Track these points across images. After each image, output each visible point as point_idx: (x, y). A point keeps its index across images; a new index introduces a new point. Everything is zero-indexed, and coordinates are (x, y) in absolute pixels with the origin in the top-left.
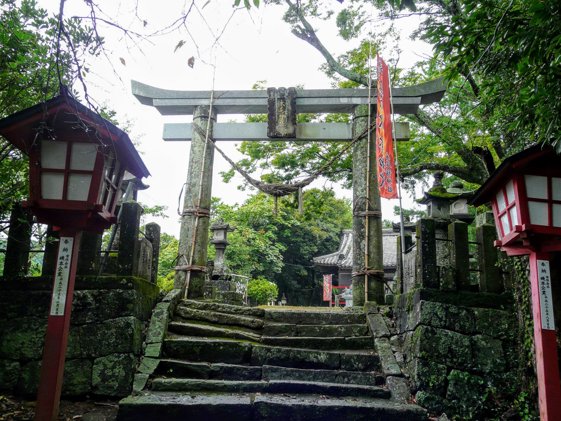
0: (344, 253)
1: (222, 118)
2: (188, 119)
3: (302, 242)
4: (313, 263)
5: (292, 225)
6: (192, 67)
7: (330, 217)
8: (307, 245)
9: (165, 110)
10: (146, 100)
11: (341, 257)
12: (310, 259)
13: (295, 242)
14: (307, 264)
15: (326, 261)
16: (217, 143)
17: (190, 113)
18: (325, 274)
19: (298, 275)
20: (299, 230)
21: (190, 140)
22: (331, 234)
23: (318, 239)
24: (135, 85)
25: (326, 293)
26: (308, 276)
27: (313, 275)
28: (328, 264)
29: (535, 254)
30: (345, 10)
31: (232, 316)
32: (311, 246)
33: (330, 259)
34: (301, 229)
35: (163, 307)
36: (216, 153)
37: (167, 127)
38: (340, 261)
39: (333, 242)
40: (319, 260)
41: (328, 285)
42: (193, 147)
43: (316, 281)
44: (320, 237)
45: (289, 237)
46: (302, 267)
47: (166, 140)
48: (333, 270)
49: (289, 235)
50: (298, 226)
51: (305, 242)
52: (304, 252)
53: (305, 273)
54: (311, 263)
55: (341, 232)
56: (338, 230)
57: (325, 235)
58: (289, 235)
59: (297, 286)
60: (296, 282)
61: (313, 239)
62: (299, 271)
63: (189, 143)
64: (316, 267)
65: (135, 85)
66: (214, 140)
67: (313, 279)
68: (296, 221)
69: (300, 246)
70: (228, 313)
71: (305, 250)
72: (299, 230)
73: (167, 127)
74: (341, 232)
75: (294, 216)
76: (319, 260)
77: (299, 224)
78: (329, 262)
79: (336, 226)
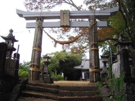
0: (83, 65)
1: (45, 21)
2: (34, 21)
6: (16, 9)
9: (27, 18)
10: (21, 15)
11: (82, 66)
16: (44, 29)
17: (35, 19)
21: (35, 28)
24: (17, 10)
29: (21, 72)
31: (45, 88)
35: (19, 85)
36: (43, 31)
37: (27, 24)
42: (35, 30)
47: (27, 28)
63: (34, 29)
65: (17, 10)
66: (43, 28)
70: (45, 87)
73: (27, 24)
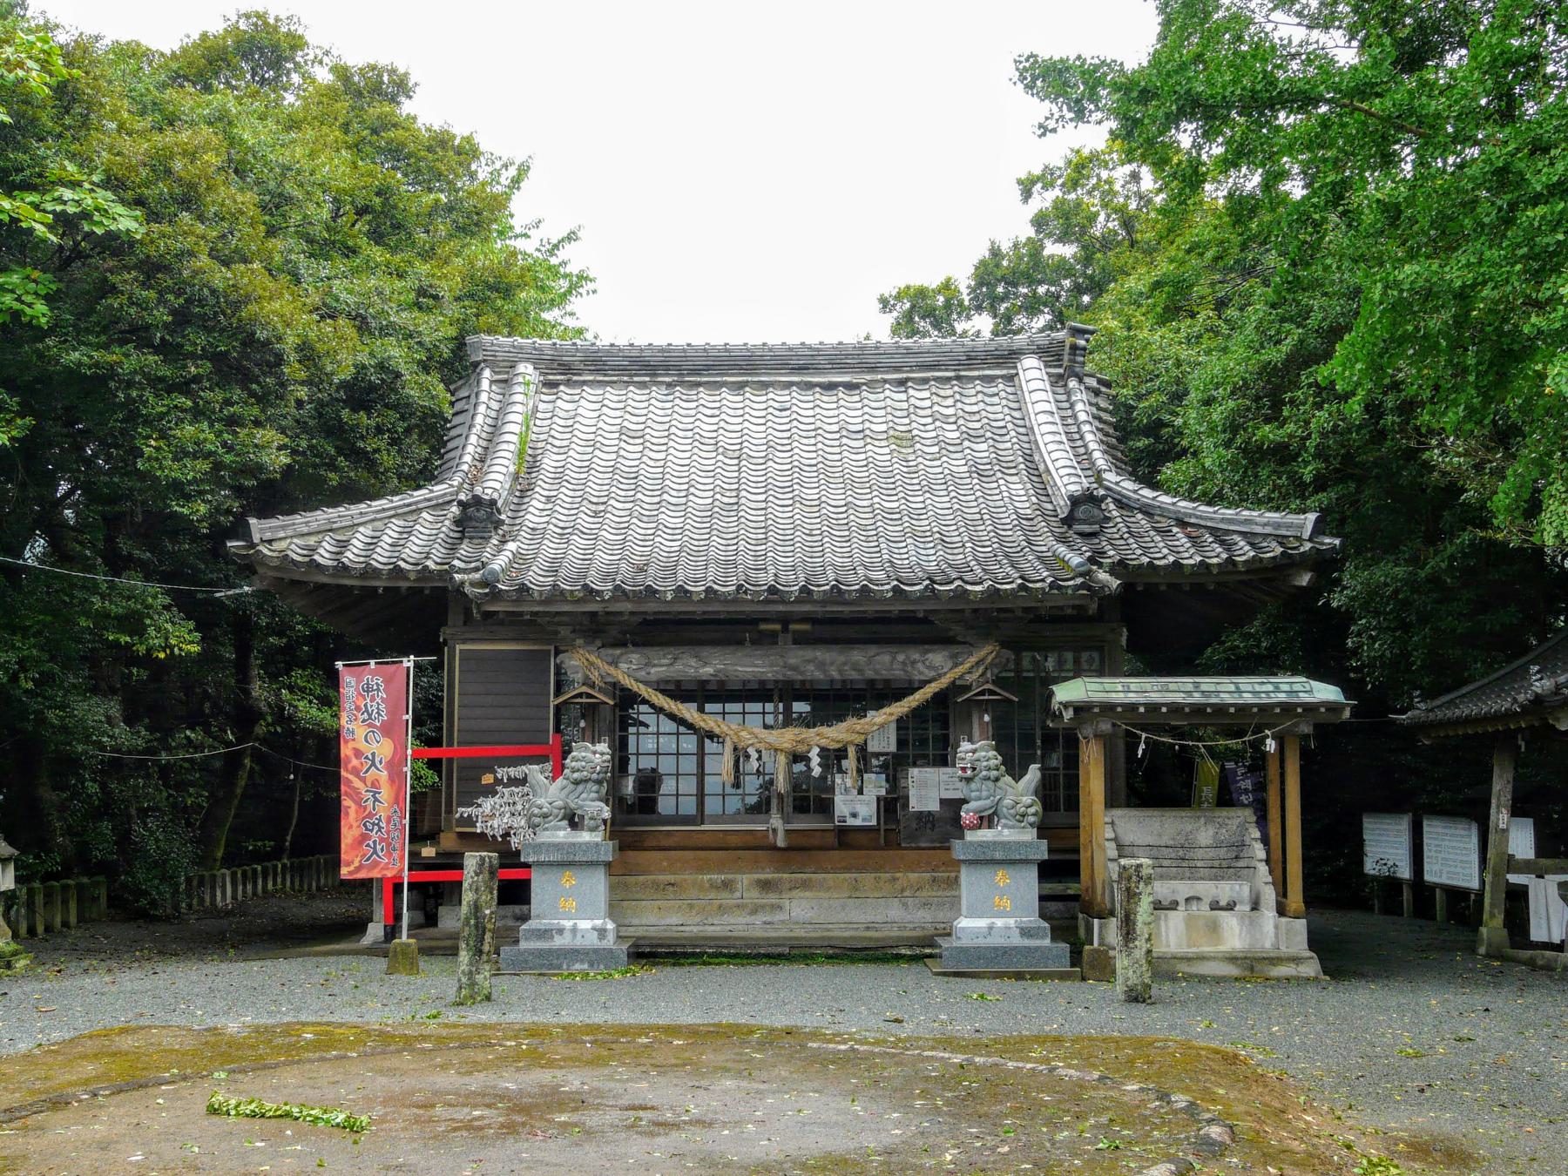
0: (496, 484)
3: (155, 382)
4: (249, 567)
5: (65, 223)
7: (377, 237)
8: (198, 414)
12: (220, 534)
13: (97, 383)
14: (196, 561)
15: (357, 543)
18: (359, 652)
19: (126, 656)
20: (126, 280)
22: (396, 352)
23: (293, 369)
25: (366, 817)
26: (207, 658)
27: (243, 651)
28: (369, 572)
30: (297, 43)
32: (233, 422)
33: (385, 535)
34: (152, 269)
38: (465, 549)
39: (404, 408)
40: (288, 537)
41: (383, 749)
43: (259, 690)
44: (307, 353)
45: (40, 334)
46: (156, 595)
48: (407, 615)
49: (40, 311)
50: (115, 244)
51: (185, 387)
52: (172, 470)
53: (184, 640)
54: (228, 558)
55: (460, 344)
56: (436, 328)
57: (347, 356)
58: (40, 311)
59: (123, 735)
60: (115, 709)
61: (246, 362)
62: (134, 623)
64: (263, 596)
67: (244, 678)
68: (104, 197)
69: (133, 417)
71: (183, 448)
72: (126, 280)
74: (460, 344)
75: (85, 162)
76: (288, 537)
77: (126, 221)
78: (380, 558)
79: (425, 299)
